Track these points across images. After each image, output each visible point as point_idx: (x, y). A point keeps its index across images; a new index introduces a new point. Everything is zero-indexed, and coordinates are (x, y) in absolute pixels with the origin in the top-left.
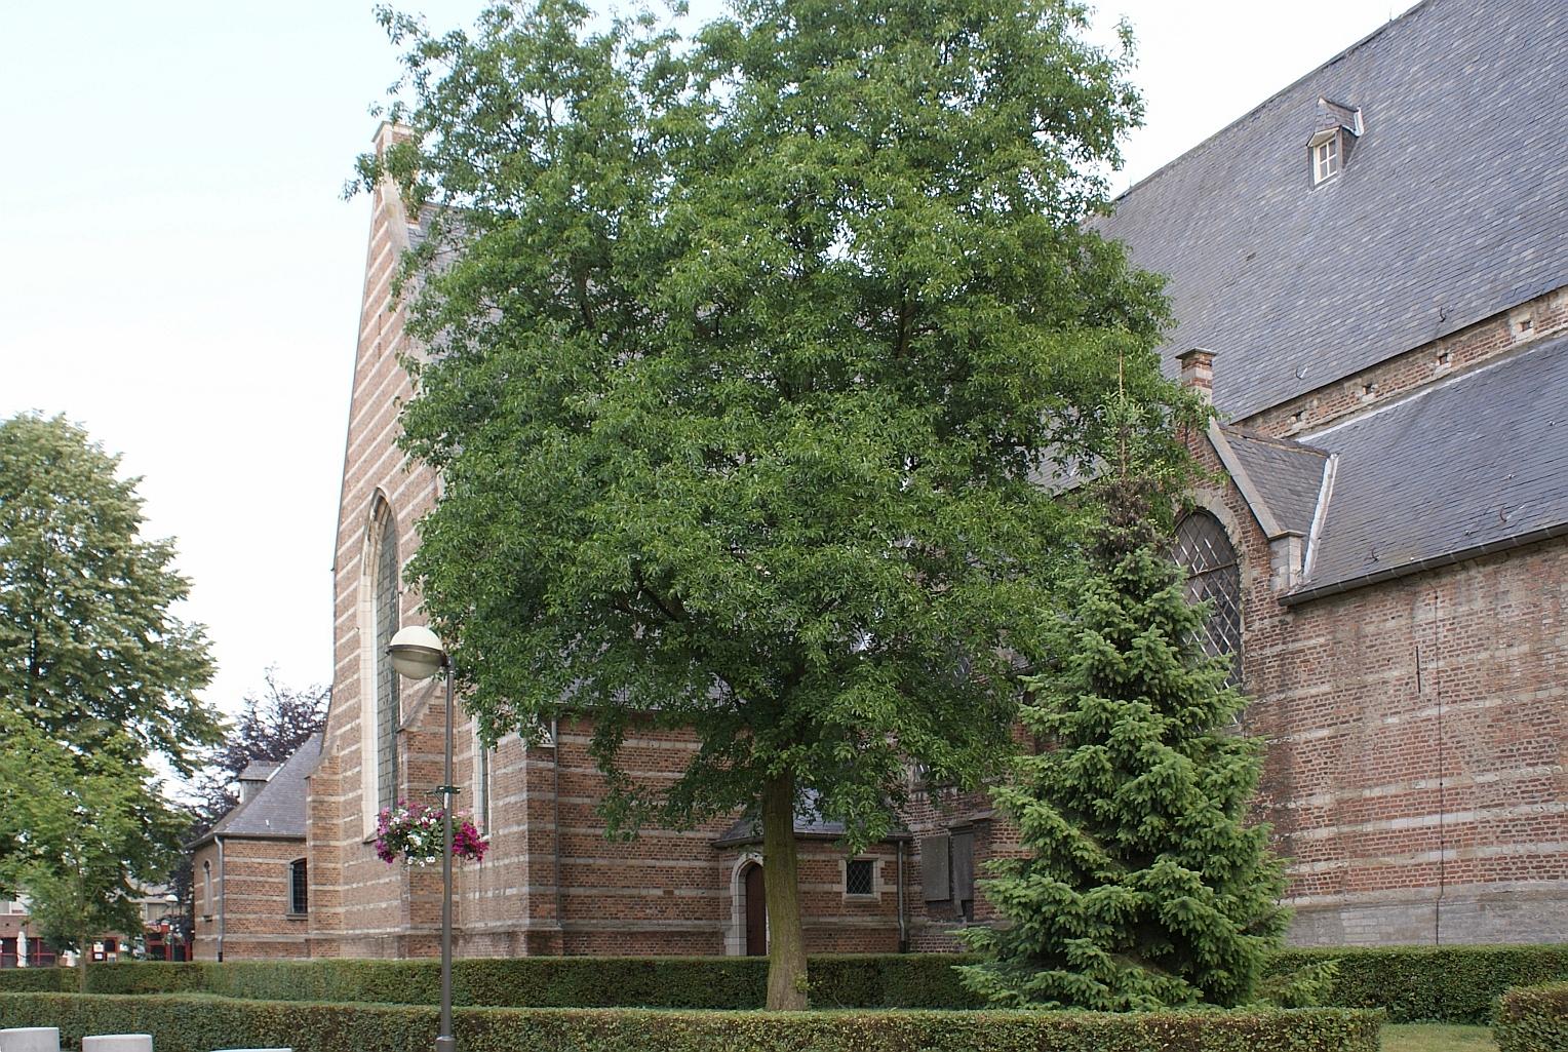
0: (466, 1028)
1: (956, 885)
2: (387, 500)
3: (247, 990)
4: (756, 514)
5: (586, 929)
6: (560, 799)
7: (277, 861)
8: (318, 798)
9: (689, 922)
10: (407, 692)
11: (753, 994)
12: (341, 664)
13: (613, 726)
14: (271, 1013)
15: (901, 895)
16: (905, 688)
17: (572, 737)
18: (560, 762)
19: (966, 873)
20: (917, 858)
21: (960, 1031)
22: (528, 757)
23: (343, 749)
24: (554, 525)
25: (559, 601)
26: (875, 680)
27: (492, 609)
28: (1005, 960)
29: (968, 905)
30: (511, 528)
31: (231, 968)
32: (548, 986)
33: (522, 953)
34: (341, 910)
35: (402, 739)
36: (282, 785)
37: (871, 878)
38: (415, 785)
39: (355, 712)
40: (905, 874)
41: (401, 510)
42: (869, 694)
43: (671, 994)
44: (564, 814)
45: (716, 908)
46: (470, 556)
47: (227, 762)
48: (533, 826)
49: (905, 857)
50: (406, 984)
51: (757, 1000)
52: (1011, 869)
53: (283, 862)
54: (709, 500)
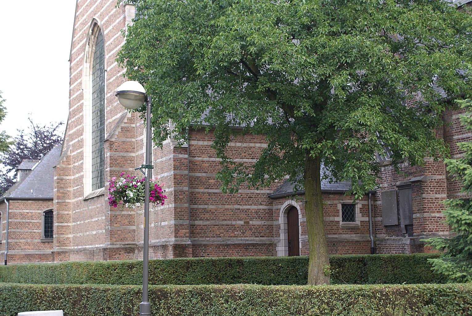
0: (156, 297)
1: (402, 217)
2: (99, 24)
3: (22, 280)
4: (305, 20)
5: (204, 243)
6: (191, 174)
7: (37, 211)
8: (60, 177)
9: (257, 238)
10: (109, 121)
11: (296, 277)
12: (73, 108)
13: (223, 134)
14: (44, 291)
15: (371, 222)
16: (383, 110)
17: (196, 142)
18: (190, 154)
19: (407, 210)
20: (379, 203)
21: (448, 296)
22: (174, 152)
23: (73, 152)
24: (198, 29)
25: (202, 68)
26: (369, 105)
27: (165, 73)
28: (455, 256)
29: (409, 227)
30: (176, 31)
31: (13, 268)
32: (187, 274)
33: (170, 256)
34: (70, 236)
35: (107, 145)
36: (40, 171)
37: (354, 213)
38: (114, 168)
39: (80, 133)
40: (373, 211)
41: (106, 29)
42: (367, 112)
43: (252, 277)
44: (193, 182)
45: (271, 230)
46: (154, 46)
47: (8, 162)
48: (177, 189)
49: (372, 202)
50: (111, 274)
51: (303, 279)
52: (457, 204)
53: (39, 211)
54: (280, 14)
